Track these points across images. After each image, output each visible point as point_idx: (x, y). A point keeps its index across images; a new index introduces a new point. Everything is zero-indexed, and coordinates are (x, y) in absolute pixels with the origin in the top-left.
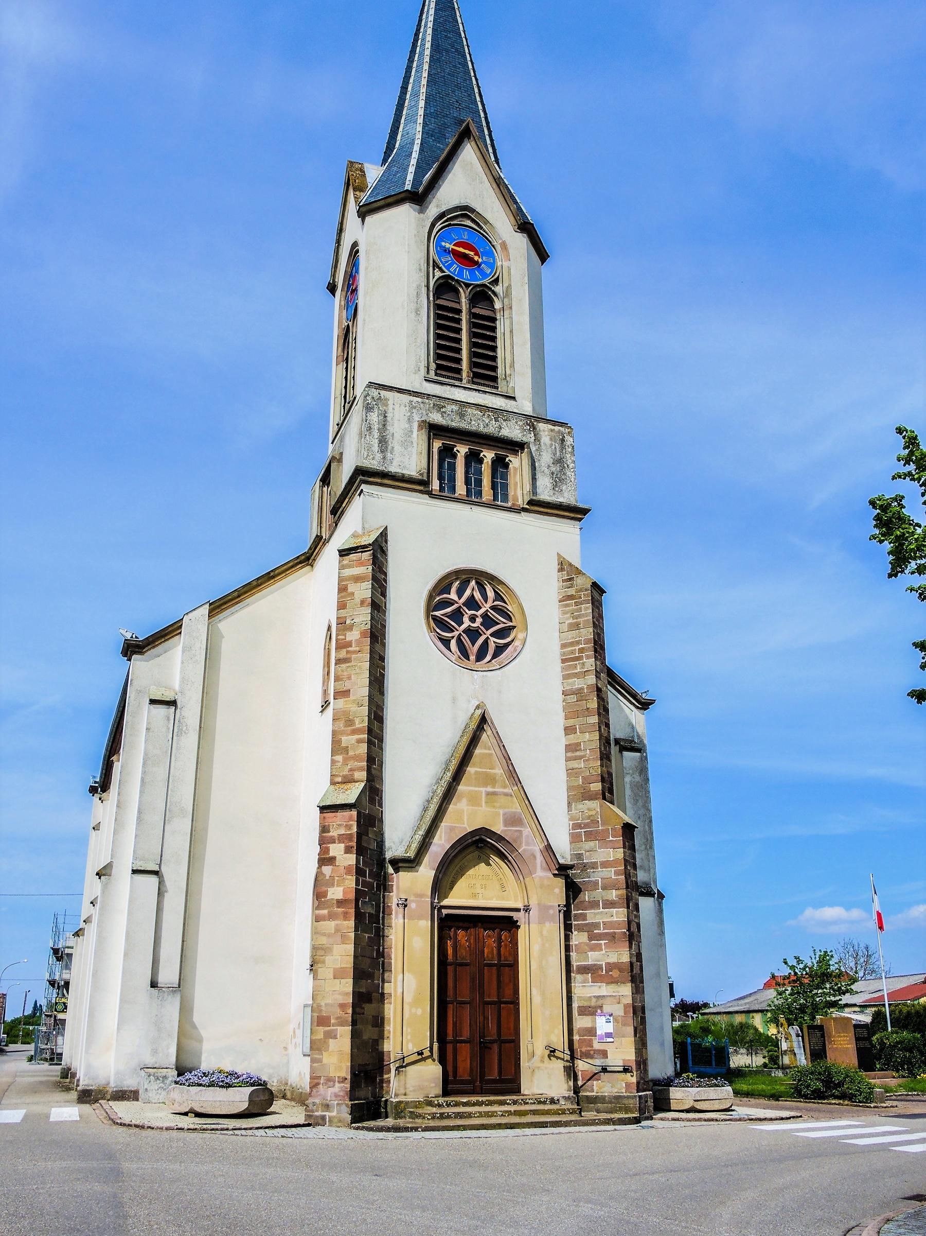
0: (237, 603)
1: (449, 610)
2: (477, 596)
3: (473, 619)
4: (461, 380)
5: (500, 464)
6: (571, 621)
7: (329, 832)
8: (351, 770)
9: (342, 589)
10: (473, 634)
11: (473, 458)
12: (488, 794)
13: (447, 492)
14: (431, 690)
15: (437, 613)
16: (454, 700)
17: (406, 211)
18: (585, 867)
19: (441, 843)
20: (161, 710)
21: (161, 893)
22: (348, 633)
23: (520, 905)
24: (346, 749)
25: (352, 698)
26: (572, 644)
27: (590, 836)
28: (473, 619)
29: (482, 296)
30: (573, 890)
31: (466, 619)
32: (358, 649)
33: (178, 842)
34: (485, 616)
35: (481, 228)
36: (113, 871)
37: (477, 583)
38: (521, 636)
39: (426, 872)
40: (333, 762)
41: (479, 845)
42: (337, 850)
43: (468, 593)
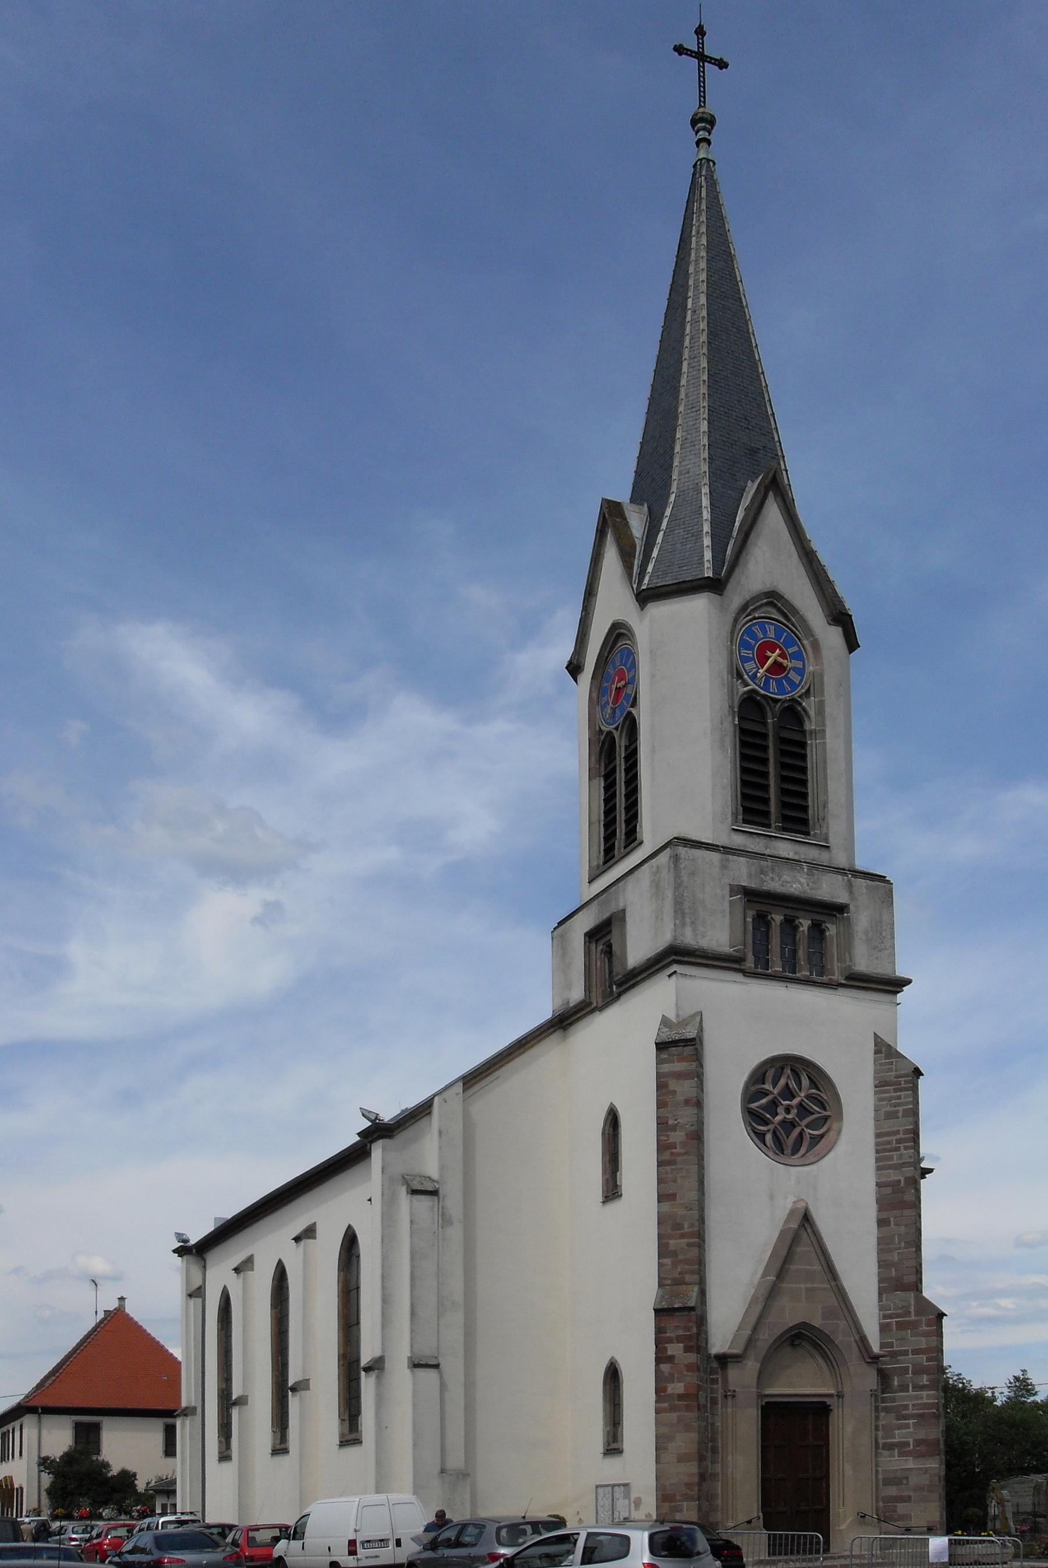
0: (487, 1076)
1: (764, 1101)
2: (793, 1084)
3: (788, 1110)
4: (768, 826)
5: (818, 929)
6: (888, 1109)
7: (666, 1333)
8: (680, 1273)
9: (662, 1086)
10: (789, 1125)
11: (790, 924)
12: (807, 1290)
13: (761, 972)
14: (750, 1193)
15: (753, 1106)
16: (772, 1197)
17: (699, 605)
18: (894, 1355)
19: (766, 1337)
20: (424, 1201)
21: (443, 1386)
22: (672, 1134)
23: (832, 1391)
24: (674, 1254)
25: (678, 1201)
26: (888, 1134)
27: (901, 1326)
28: (788, 1110)
29: (793, 714)
30: (884, 1376)
31: (780, 1109)
32: (683, 1151)
33: (453, 1336)
34: (800, 1105)
35: (789, 620)
36: (386, 1366)
37: (792, 1070)
38: (835, 1126)
39: (752, 1365)
40: (660, 1265)
41: (801, 1338)
42: (675, 1349)
43: (782, 1082)
